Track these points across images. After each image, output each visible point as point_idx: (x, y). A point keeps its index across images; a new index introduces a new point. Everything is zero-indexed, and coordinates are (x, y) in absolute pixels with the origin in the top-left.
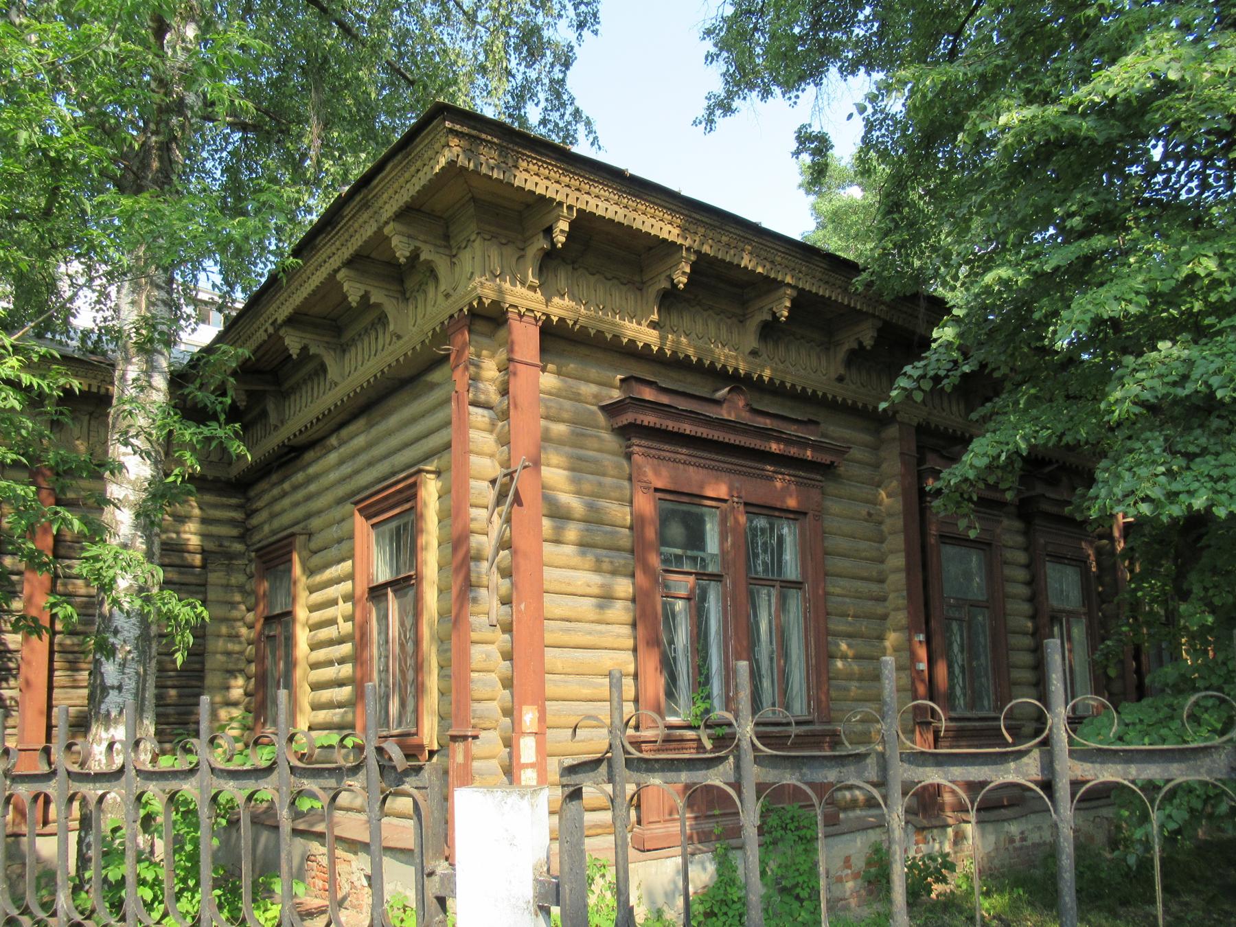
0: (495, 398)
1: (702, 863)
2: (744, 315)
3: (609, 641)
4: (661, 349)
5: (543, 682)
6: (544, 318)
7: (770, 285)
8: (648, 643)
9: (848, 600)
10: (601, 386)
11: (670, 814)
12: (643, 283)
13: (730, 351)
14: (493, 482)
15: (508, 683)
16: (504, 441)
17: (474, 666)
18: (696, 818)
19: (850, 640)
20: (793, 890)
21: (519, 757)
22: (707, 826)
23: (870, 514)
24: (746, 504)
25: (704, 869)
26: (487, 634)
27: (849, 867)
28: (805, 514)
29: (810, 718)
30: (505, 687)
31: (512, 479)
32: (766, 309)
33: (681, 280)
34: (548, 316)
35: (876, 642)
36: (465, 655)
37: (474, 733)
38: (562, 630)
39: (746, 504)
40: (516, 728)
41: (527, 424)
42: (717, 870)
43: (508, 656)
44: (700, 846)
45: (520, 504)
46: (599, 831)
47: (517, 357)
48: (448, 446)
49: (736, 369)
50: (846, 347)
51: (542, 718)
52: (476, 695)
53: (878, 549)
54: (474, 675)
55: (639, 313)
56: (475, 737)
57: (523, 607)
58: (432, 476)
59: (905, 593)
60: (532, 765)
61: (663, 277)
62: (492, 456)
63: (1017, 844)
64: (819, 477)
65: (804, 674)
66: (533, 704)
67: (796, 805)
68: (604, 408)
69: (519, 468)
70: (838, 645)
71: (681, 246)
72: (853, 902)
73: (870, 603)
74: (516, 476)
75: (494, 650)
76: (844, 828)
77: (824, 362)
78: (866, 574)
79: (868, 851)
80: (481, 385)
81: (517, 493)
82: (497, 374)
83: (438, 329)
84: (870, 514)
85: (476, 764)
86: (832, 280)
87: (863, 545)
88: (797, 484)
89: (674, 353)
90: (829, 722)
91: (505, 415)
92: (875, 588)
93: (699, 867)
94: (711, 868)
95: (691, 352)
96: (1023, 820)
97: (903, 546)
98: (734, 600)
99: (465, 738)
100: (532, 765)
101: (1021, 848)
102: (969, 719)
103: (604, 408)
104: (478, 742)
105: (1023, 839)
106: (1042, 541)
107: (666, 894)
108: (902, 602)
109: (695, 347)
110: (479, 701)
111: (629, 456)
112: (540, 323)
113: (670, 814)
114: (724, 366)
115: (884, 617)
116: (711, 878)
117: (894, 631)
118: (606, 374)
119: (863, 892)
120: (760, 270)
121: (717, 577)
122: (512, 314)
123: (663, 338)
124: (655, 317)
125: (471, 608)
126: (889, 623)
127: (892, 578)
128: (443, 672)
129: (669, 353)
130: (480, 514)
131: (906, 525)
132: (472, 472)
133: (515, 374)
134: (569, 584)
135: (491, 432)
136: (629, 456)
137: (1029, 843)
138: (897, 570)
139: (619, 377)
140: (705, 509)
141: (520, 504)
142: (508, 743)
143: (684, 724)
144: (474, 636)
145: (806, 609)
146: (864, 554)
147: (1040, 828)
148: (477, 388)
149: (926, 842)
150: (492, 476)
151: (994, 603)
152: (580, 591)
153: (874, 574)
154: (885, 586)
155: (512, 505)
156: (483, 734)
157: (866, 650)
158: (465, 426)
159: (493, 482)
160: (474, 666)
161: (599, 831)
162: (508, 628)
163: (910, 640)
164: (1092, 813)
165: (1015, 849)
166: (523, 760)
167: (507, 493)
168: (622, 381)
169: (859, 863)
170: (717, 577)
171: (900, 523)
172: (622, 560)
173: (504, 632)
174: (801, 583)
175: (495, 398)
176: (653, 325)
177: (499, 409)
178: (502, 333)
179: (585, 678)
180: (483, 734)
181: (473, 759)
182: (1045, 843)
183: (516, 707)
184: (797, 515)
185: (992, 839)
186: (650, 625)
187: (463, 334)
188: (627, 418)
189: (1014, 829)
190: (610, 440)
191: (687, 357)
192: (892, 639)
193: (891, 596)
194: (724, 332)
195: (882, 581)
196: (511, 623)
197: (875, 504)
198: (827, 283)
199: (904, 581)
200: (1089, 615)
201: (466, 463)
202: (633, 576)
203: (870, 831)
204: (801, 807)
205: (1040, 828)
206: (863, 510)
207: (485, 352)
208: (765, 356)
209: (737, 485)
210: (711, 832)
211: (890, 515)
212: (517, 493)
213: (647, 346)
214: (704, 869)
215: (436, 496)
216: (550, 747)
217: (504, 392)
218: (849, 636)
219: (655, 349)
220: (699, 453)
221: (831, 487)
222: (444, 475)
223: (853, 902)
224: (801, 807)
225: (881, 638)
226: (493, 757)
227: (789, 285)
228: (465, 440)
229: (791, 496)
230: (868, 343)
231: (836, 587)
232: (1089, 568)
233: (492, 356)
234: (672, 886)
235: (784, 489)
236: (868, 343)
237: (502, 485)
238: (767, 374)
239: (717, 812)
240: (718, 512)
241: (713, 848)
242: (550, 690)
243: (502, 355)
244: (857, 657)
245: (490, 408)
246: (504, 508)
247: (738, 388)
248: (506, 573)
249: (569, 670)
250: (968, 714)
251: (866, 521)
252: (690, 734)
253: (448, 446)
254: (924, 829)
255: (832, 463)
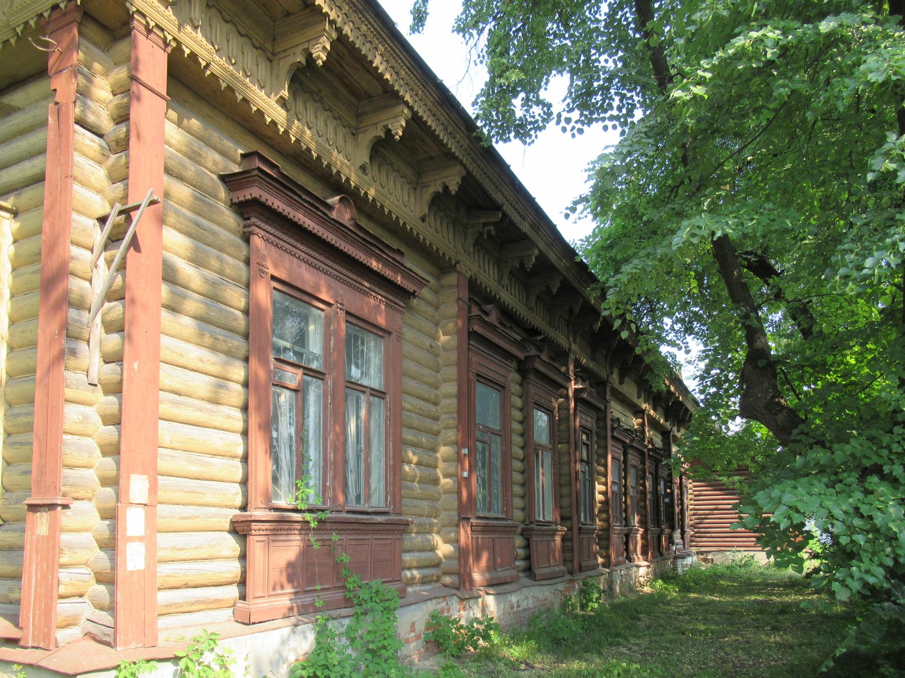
0: (105, 122)
1: (304, 633)
2: (357, 129)
3: (217, 420)
4: (286, 132)
5: (155, 455)
6: (174, 44)
7: (391, 96)
8: (260, 426)
9: (413, 415)
10: (226, 154)
11: (274, 589)
12: (274, 54)
13: (347, 160)
14: (103, 220)
15: (113, 450)
16: (120, 176)
17: (67, 427)
18: (296, 593)
19: (413, 449)
20: (377, 651)
21: (125, 529)
22: (308, 599)
23: (431, 346)
24: (347, 313)
25: (306, 638)
26: (87, 394)
27: (413, 631)
28: (389, 333)
29: (387, 509)
30: (105, 454)
31: (129, 220)
32: (380, 126)
33: (320, 55)
34: (179, 43)
35: (431, 453)
36: (54, 414)
37: (65, 502)
38: (171, 402)
39: (347, 313)
40: (123, 497)
41: (146, 161)
42: (316, 639)
43: (115, 420)
44: (300, 618)
45: (138, 249)
46: (202, 607)
47: (142, 77)
48: (39, 179)
49: (348, 180)
50: (432, 190)
51: (153, 489)
52: (69, 460)
53: (436, 377)
54: (66, 437)
55: (268, 85)
56: (65, 507)
57: (136, 365)
58: (7, 215)
59: (455, 415)
60: (141, 539)
61: (299, 50)
62: (99, 192)
63: (515, 609)
64: (401, 304)
65: (383, 472)
66: (142, 473)
67: (379, 581)
68: (224, 178)
69: (144, 202)
70: (406, 452)
71: (327, 15)
72: (416, 659)
73: (429, 420)
74: (135, 215)
75: (93, 415)
76: (411, 600)
77: (412, 200)
78: (426, 396)
79: (427, 617)
80: (89, 102)
81: (135, 238)
82: (111, 97)
83: (32, 23)
84: (431, 346)
85: (64, 537)
86: (438, 114)
87: (426, 371)
88: (387, 305)
89: (298, 141)
90: (401, 514)
91: (122, 145)
92: (433, 408)
93: (302, 636)
94: (311, 637)
95: (313, 146)
96: (519, 592)
97: (455, 377)
98: (333, 398)
99: (52, 507)
100: (141, 539)
101: (517, 612)
102: (487, 518)
103: (224, 178)
104: (67, 511)
105: (518, 606)
106: (532, 392)
107: (271, 663)
108: (453, 422)
109: (316, 142)
110: (71, 467)
111: (246, 238)
112: (169, 50)
113: (274, 589)
114: (338, 172)
115: (437, 434)
116: (311, 645)
117: (445, 445)
118: (228, 144)
119: (422, 650)
120: (387, 76)
121: (318, 374)
122: (138, 23)
123: (290, 122)
124: (285, 93)
125: (71, 362)
126: (440, 438)
127: (444, 402)
128: (11, 439)
129: (293, 139)
130: (81, 258)
131: (459, 358)
132: (75, 203)
133: (138, 98)
134: (181, 355)
135: (100, 163)
136: (246, 238)
137: (521, 609)
138: (449, 396)
139: (241, 151)
140: (314, 310)
141: (138, 249)
142: (111, 515)
143: (290, 507)
144: (69, 393)
145: (387, 417)
146: (425, 379)
147: (527, 598)
148: (85, 105)
149: (464, 609)
150: (101, 213)
151: (504, 433)
152: (191, 366)
153: (432, 396)
154: (438, 408)
155: (128, 249)
156: (75, 505)
157: (426, 458)
158: (65, 144)
159: (103, 220)
160: (67, 427)
161: (202, 607)
162: (115, 389)
163: (458, 453)
164: (553, 587)
165: (514, 613)
166: (129, 533)
167: (118, 232)
168: (243, 156)
169: (421, 627)
170: (318, 374)
171: (454, 357)
172: (238, 343)
173: (106, 393)
174: (384, 393)
175: (105, 122)
176: (282, 102)
177: (112, 137)
178: (121, 48)
179: (194, 456)
180: (75, 505)
181: (62, 531)
182: (529, 609)
183: (123, 473)
184: (382, 332)
185: (502, 606)
186: (257, 407)
187: (70, 31)
188: (254, 192)
189: (513, 598)
190: (230, 218)
191: (309, 150)
192: (444, 451)
193: (443, 417)
194: (340, 138)
195: (436, 404)
196: (121, 382)
197: (435, 339)
198: (434, 115)
199: (455, 405)
200: (554, 449)
201: (66, 191)
202: (246, 360)
203: (429, 602)
204: (383, 582)
205: (527, 598)
206: (428, 342)
207: (97, 66)
208: (370, 176)
209: (341, 292)
210: (313, 604)
211: (445, 350)
212: (135, 238)
213: (273, 123)
214: (306, 638)
215: (11, 239)
216: (161, 523)
217: (122, 117)
218: (414, 445)
219: (282, 130)
220: (311, 252)
221: (407, 316)
222: (21, 217)
223: (416, 659)
224: (383, 582)
225: (434, 450)
226: (86, 530)
227: (407, 103)
228: (67, 164)
229: (381, 314)
230: (454, 188)
231: (409, 403)
232: (554, 417)
233: (106, 74)
234: (277, 656)
235: (376, 307)
236: (454, 188)
237: (116, 226)
238: (372, 193)
239: (318, 587)
240: (323, 314)
241: (313, 619)
242: (162, 465)
243: (121, 73)
244: (419, 464)
245: (101, 136)
246: (117, 253)
247: (347, 200)
248: (115, 327)
249: (178, 445)
250: (487, 515)
251: (428, 351)
252: (297, 516)
253: (39, 179)
254: (464, 600)
255: (415, 292)
